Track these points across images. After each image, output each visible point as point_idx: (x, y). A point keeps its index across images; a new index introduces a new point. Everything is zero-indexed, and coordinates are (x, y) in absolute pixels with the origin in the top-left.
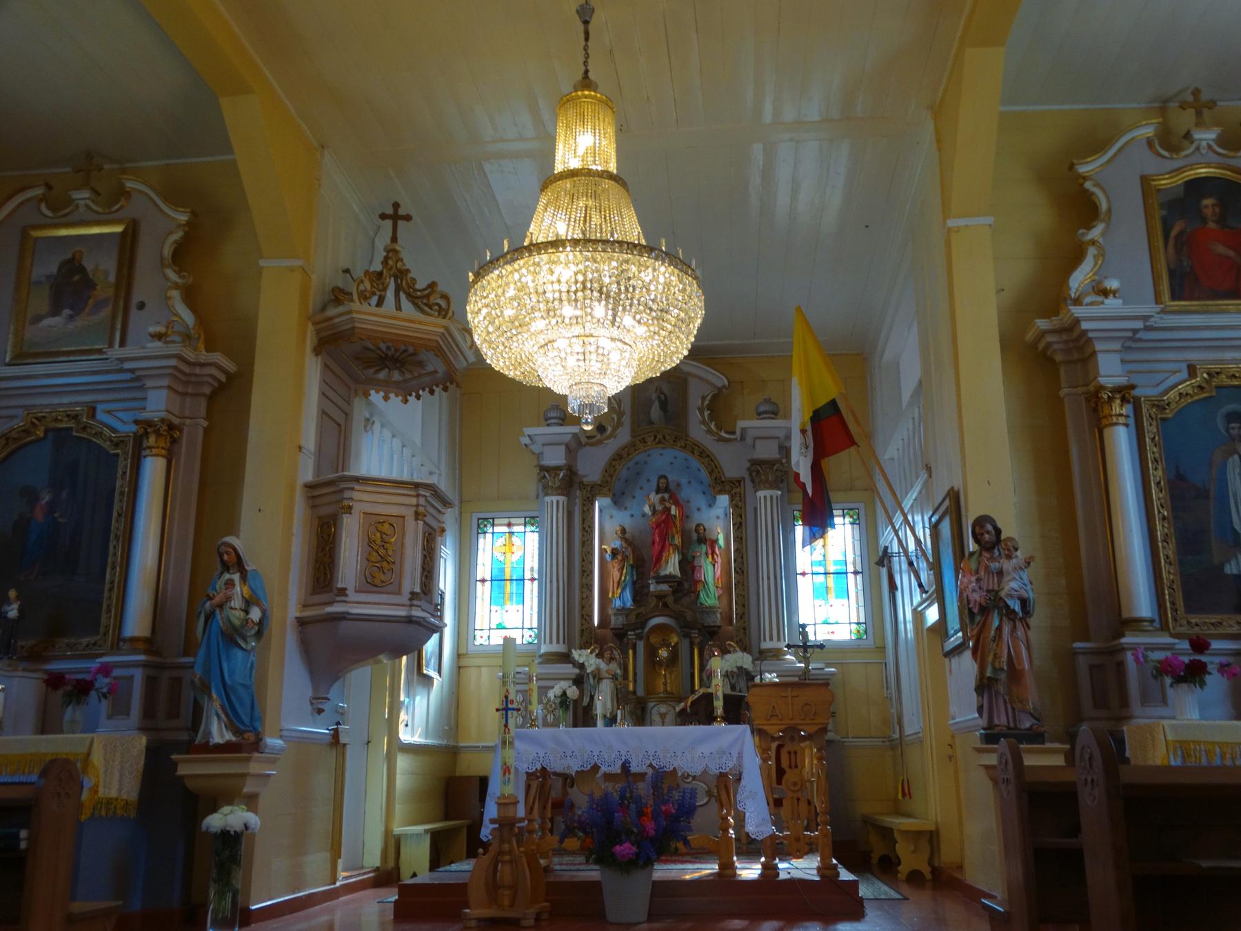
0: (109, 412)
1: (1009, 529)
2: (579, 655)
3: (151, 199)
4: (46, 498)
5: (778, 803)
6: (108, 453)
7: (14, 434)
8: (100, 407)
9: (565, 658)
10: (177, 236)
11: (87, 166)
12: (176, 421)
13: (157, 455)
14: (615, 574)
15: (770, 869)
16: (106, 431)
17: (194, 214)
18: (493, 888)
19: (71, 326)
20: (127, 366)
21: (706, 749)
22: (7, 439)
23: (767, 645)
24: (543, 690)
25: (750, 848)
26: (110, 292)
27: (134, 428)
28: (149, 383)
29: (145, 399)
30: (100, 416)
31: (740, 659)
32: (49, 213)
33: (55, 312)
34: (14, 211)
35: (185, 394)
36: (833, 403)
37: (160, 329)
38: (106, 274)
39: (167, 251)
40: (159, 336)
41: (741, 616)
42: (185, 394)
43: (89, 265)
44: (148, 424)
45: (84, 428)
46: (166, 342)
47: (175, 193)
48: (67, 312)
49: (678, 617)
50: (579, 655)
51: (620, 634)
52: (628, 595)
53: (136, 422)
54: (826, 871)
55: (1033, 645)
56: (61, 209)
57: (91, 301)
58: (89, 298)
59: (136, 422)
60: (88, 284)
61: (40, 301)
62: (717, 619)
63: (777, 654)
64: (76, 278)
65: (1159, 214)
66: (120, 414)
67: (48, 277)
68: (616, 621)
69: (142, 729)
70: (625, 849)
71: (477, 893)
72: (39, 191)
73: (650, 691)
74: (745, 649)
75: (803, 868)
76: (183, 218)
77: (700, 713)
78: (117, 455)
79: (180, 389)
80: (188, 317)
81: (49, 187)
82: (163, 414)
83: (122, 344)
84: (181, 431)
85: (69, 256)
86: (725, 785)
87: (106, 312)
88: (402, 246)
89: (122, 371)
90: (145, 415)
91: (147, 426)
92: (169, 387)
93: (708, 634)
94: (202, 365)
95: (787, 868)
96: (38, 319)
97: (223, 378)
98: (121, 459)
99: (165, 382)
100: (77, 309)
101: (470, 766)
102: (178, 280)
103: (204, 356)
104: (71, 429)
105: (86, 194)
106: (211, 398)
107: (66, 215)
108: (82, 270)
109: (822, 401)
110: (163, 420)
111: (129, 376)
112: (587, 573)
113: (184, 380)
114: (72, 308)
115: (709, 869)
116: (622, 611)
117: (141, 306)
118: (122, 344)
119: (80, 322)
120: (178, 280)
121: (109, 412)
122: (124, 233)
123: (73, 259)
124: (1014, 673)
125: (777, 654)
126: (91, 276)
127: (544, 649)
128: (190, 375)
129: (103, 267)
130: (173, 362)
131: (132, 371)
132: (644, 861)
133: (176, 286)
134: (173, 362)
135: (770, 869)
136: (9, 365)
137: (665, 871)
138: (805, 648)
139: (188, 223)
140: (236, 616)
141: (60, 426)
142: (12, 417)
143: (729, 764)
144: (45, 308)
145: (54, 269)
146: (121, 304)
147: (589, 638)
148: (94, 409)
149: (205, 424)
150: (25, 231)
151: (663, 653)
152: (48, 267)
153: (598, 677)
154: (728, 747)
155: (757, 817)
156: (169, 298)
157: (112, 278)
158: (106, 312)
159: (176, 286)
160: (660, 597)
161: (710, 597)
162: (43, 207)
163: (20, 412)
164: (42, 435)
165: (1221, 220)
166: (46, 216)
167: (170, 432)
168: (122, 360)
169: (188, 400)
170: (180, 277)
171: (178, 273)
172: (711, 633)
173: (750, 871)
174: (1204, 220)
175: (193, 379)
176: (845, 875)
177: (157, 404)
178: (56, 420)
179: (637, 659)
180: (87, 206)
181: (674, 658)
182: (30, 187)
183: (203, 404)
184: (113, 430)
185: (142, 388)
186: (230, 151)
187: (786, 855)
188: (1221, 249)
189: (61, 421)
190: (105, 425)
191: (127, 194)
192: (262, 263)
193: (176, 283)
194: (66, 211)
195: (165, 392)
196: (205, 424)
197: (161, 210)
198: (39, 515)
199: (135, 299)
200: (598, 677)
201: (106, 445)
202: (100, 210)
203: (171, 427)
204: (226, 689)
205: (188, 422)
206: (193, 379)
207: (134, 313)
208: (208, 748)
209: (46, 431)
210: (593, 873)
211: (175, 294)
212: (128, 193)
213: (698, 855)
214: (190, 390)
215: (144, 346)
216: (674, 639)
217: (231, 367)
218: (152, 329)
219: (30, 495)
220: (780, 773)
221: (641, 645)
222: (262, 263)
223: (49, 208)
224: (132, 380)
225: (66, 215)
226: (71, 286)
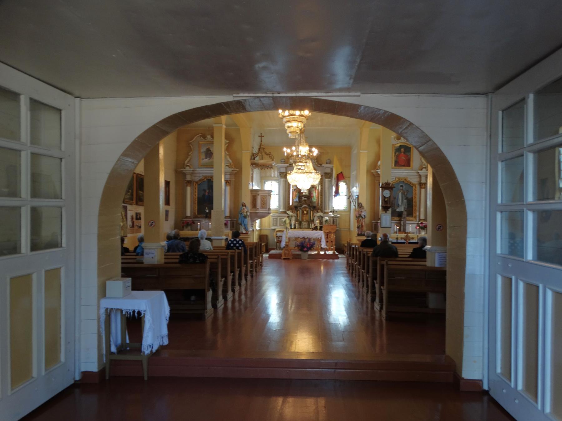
1: (364, 205)
2: (288, 212)
4: (207, 191)
5: (327, 242)
9: (285, 212)
14: (295, 194)
15: (325, 252)
18: (285, 254)
21: (317, 235)
23: (326, 211)
24: (280, 219)
25: (322, 249)
31: (321, 214)
33: (206, 158)
36: (342, 173)
41: (321, 204)
49: (309, 205)
50: (288, 212)
51: (296, 207)
52: (297, 199)
54: (334, 253)
55: (366, 221)
61: (203, 156)
62: (316, 204)
63: (328, 213)
65: (394, 151)
68: (295, 204)
69: (231, 230)
70: (305, 249)
71: (283, 255)
73: (302, 220)
74: (322, 212)
75: (331, 252)
77: (316, 228)
86: (319, 240)
88: (263, 140)
93: (314, 208)
95: (328, 252)
96: (203, 159)
101: (264, 233)
109: (339, 172)
112: (289, 194)
115: (316, 252)
116: (296, 202)
124: (362, 226)
125: (328, 213)
127: (281, 210)
132: (307, 251)
135: (325, 252)
137: (310, 252)
138: (333, 212)
140: (245, 214)
143: (319, 237)
144: (204, 157)
147: (289, 208)
151: (305, 212)
153: (292, 216)
154: (320, 234)
155: (324, 245)
160: (305, 201)
161: (314, 200)
165: (404, 153)
172: (314, 207)
173: (322, 253)
174: (401, 152)
176: (337, 253)
179: (299, 213)
181: (307, 213)
187: (328, 250)
188: (403, 158)
198: (207, 194)
200: (292, 216)
204: (245, 225)
208: (242, 233)
210: (299, 252)
213: (315, 250)
216: (307, 209)
219: (205, 190)
220: (327, 238)
221: (301, 210)
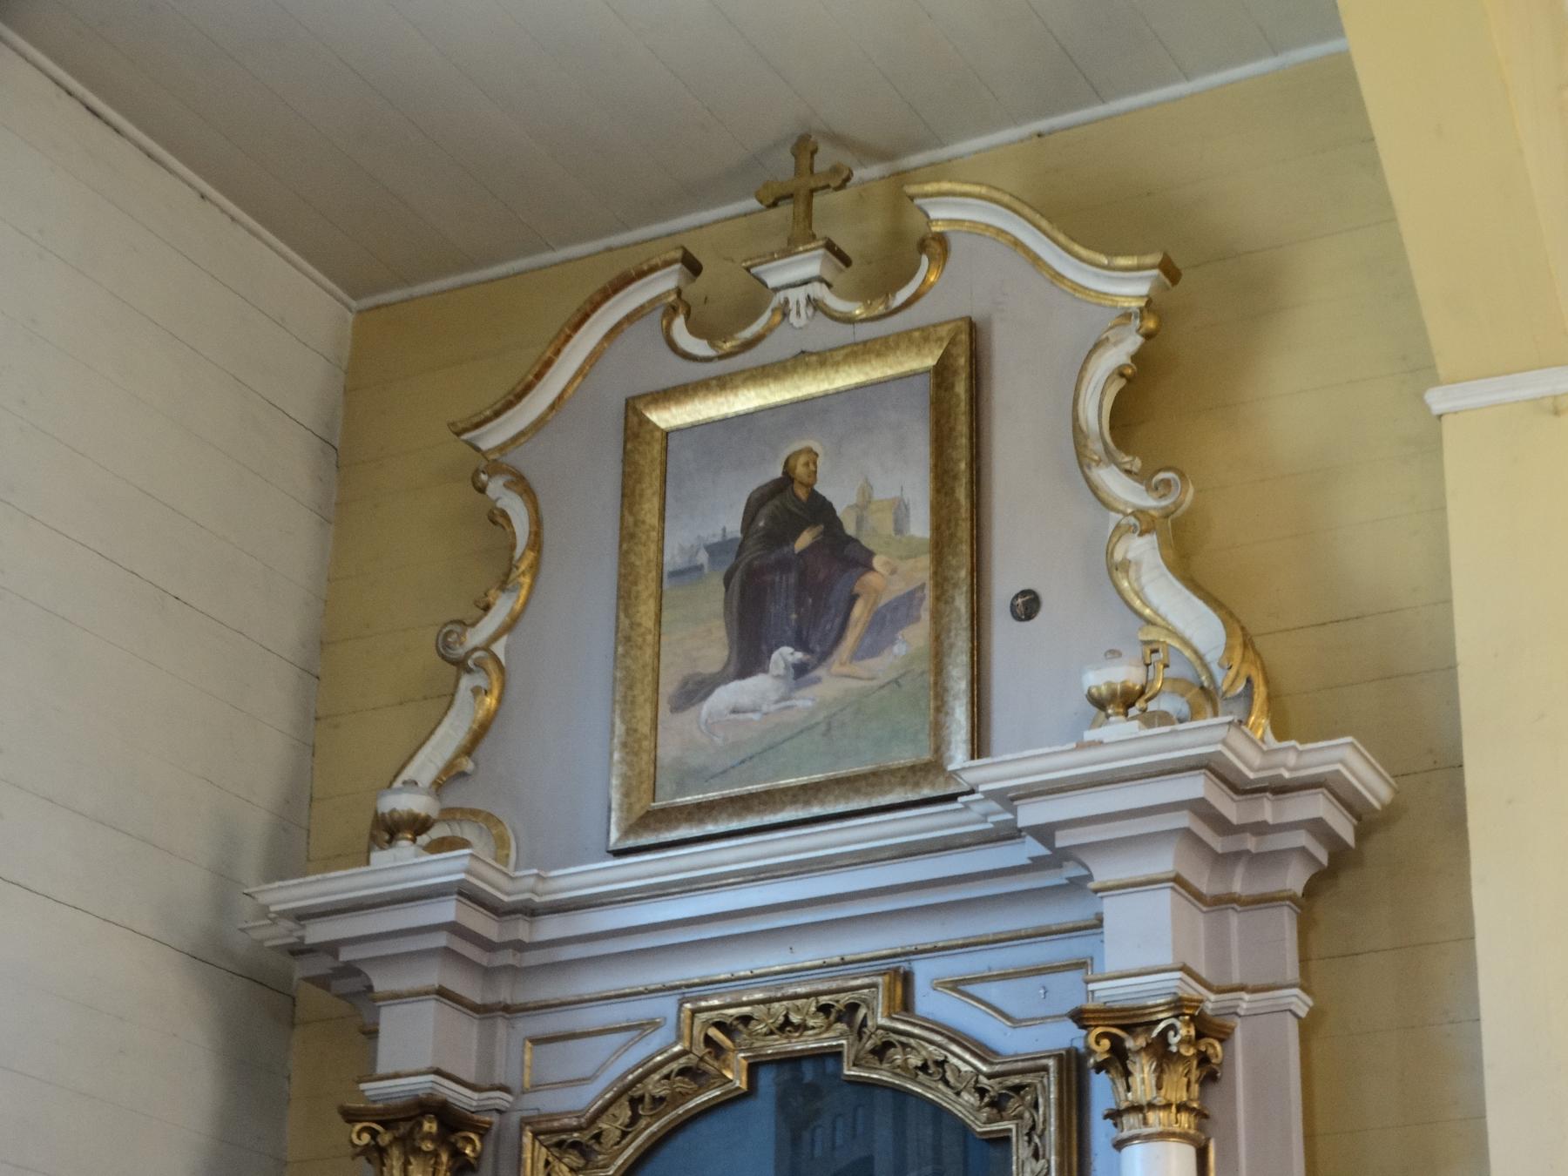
0: (956, 986)
3: (1017, 244)
6: (965, 1129)
7: (655, 1086)
8: (924, 972)
10: (1121, 352)
11: (800, 181)
12: (1211, 1003)
13: (1163, 1136)
16: (963, 1062)
17: (1170, 271)
19: (805, 700)
20: (1030, 814)
22: (635, 1102)
26: (920, 569)
27: (1068, 1036)
28: (1105, 871)
29: (1098, 923)
30: (929, 1002)
32: (699, 347)
33: (749, 661)
34: (594, 357)
35: (1220, 902)
37: (1126, 674)
38: (900, 511)
39: (1094, 410)
40: (1126, 700)
42: (1220, 902)
43: (839, 493)
44: (1131, 1020)
45: (881, 1051)
46: (1149, 719)
47: (1092, 213)
48: (785, 656)
53: (1080, 1017)
56: (727, 324)
57: (858, 610)
58: (853, 599)
59: (1080, 1017)
60: (845, 554)
61: (699, 633)
64: (804, 540)
66: (992, 992)
67: (713, 550)
72: (665, 283)
76: (1132, 289)
78: (1003, 1140)
79: (1204, 885)
80: (1198, 626)
81: (693, 267)
82: (1172, 982)
83: (979, 746)
84: (1224, 1036)
85: (777, 472)
87: (914, 638)
89: (1009, 834)
90: (1108, 992)
91: (1122, 1032)
92: (1178, 880)
94: (1281, 789)
96: (695, 690)
97: (1345, 829)
98: (1020, 1150)
99: (1163, 862)
100: (817, 641)
102: (1149, 502)
103: (1296, 759)
104: (836, 1054)
105: (809, 264)
106: (1307, 903)
107: (749, 345)
108: (821, 510)
110: (1178, 1005)
111: (1032, 848)
113: (1221, 841)
114: (800, 643)
117: (1028, 606)
118: (979, 746)
119: (835, 682)
120: (1149, 502)
121: (956, 986)
122: (941, 372)
123: (788, 478)
126: (850, 529)
128: (1242, 829)
129: (882, 489)
130: (1195, 787)
131: (1044, 833)
133: (1145, 523)
134: (1195, 787)
136: (618, 853)
139: (1150, 306)
141: (799, 1044)
142: (644, 1027)
144: (714, 650)
145: (732, 524)
146: (961, 603)
148: (907, 979)
149: (1300, 1002)
150: (633, 410)
152: (712, 515)
156: (1125, 566)
157: (920, 527)
158: (914, 638)
159: (1145, 523)
162: (679, 324)
163: (665, 1007)
164: (741, 1083)
166: (849, 320)
167: (1194, 1043)
168: (1009, 798)
169: (1234, 919)
170: (1152, 489)
171: (1142, 477)
175: (1251, 843)
177: (1143, 946)
178: (786, 1026)
180: (814, 303)
182: (642, 274)
183: (1285, 921)
184: (983, 1052)
185: (1077, 885)
186: (1333, 27)
189: (803, 1027)
190: (956, 1037)
191: (937, 245)
192: (1437, 400)
193: (1139, 513)
194: (748, 333)
195: (1164, 899)
196: (1300, 1002)
197: (539, 424)
199: (1003, 588)
201: (964, 1106)
202: (858, 311)
203: (1207, 1028)
205: (1245, 1002)
206: (1251, 843)
207: (1003, 629)
209: (753, 1069)
211: (1142, 550)
212: (941, 239)
214: (1238, 887)
215: (1050, 734)
217: (1375, 788)
218: (1100, 678)
222: (1437, 400)
223: (695, 330)
224: (1037, 864)
225: (749, 345)
226: (791, 569)
